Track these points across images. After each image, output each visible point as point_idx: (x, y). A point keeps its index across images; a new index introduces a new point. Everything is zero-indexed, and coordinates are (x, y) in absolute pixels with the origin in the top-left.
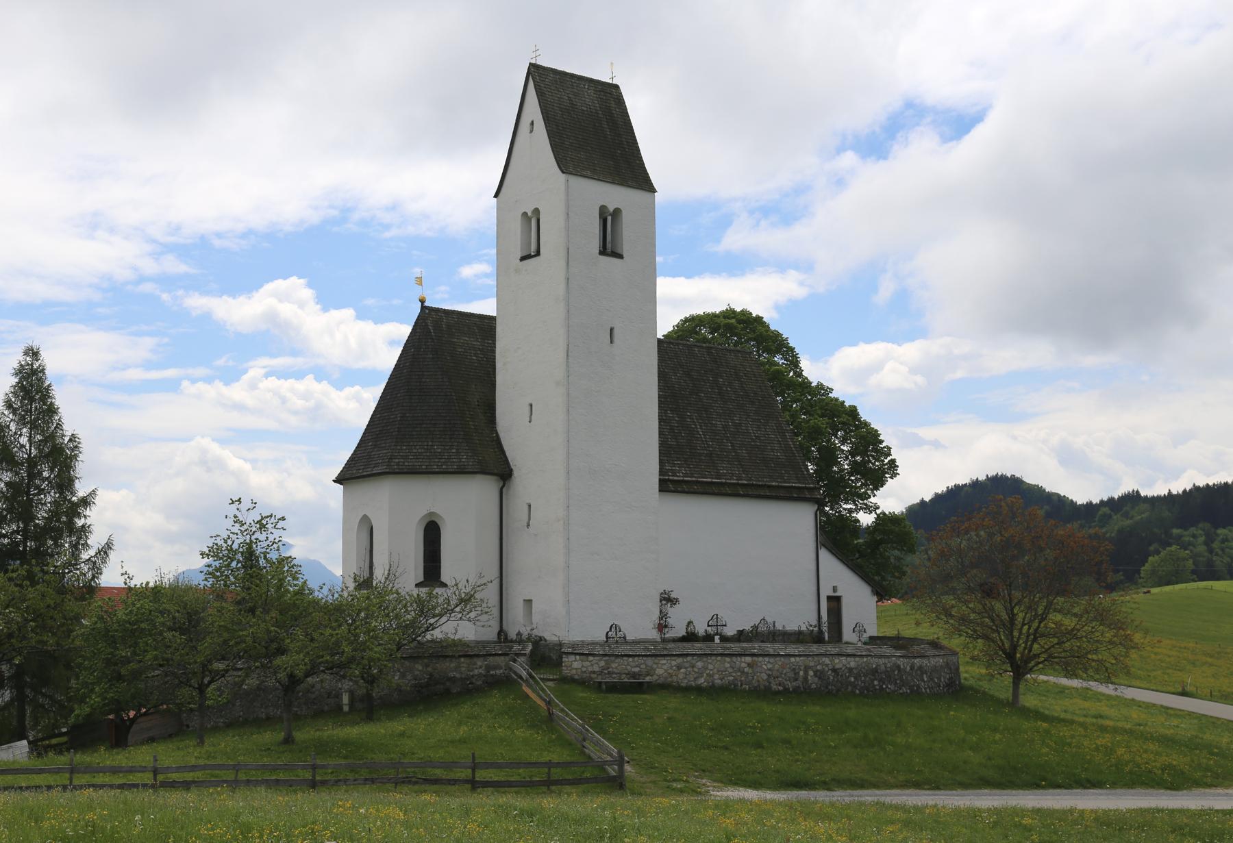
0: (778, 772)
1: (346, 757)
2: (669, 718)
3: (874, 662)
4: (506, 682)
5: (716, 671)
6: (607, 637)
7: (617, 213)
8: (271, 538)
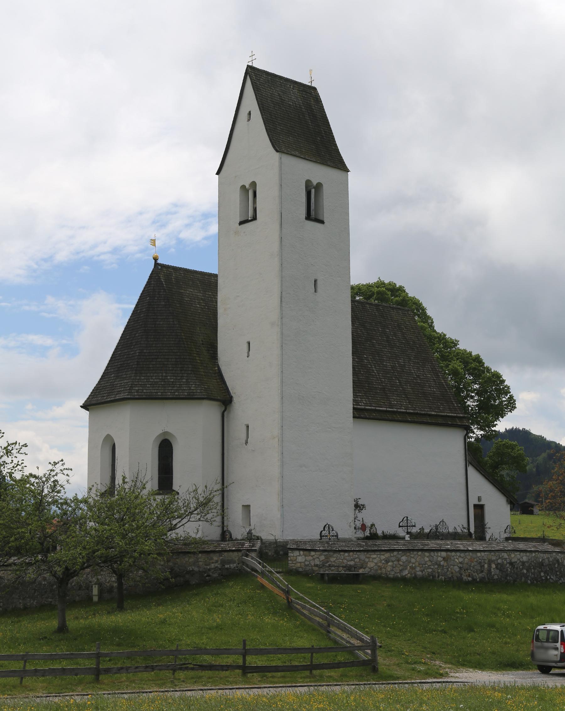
0: (493, 653)
1: (119, 645)
2: (389, 606)
3: (541, 557)
4: (240, 574)
5: (417, 565)
6: (321, 536)
7: (319, 187)
8: (15, 461)
